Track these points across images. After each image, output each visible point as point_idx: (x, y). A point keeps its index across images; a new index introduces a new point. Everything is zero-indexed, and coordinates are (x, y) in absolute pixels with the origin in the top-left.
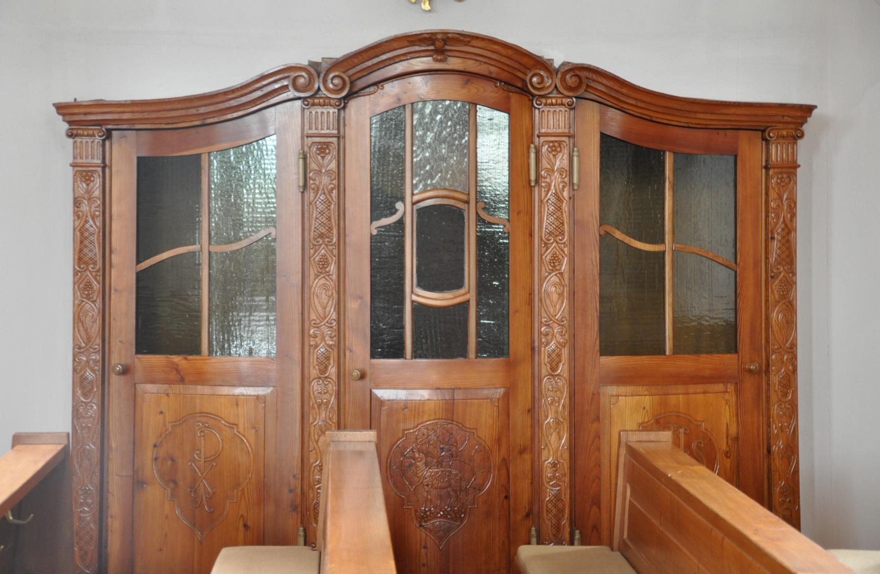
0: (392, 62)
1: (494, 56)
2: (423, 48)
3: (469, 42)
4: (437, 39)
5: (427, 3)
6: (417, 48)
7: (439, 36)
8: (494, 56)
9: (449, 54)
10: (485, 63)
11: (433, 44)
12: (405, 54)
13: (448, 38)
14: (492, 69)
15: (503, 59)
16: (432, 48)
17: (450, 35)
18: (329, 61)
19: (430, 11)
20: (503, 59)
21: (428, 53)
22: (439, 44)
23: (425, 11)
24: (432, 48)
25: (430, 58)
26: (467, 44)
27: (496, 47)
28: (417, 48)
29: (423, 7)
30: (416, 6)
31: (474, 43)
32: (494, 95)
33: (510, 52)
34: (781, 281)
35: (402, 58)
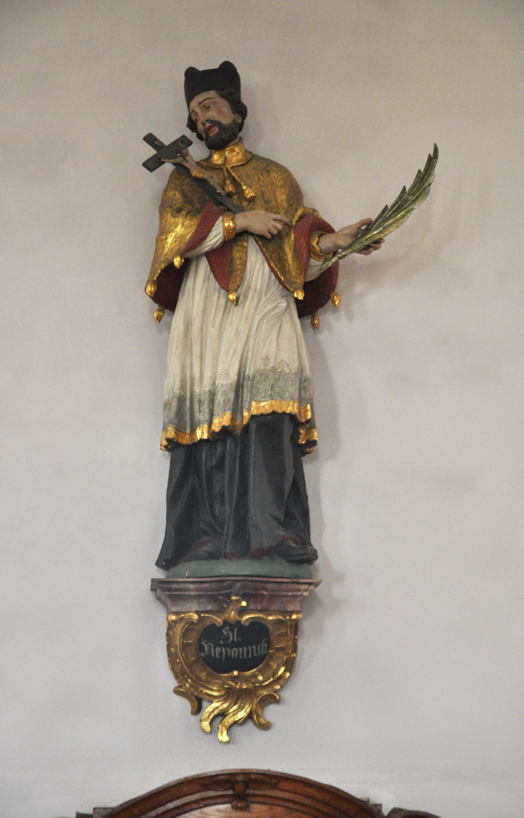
0: (181, 811)
1: (307, 801)
2: (219, 793)
3: (276, 784)
4: (237, 782)
5: (225, 732)
6: (212, 793)
7: (240, 778)
8: (307, 801)
9: (252, 799)
10: (297, 810)
11: (232, 788)
12: (197, 801)
13: (250, 779)
14: (218, 489)
15: (319, 806)
16: (230, 792)
17: (253, 777)
18: (102, 812)
19: (228, 742)
20: (319, 806)
21: (226, 799)
22: (239, 788)
23: (221, 742)
24: (230, 792)
25: (228, 806)
26: (274, 787)
27: (310, 790)
28: (212, 793)
29: (220, 738)
30: (210, 737)
31: (282, 785)
32: (272, 664)
33: (327, 797)
34: (186, 671)
35: (194, 806)
